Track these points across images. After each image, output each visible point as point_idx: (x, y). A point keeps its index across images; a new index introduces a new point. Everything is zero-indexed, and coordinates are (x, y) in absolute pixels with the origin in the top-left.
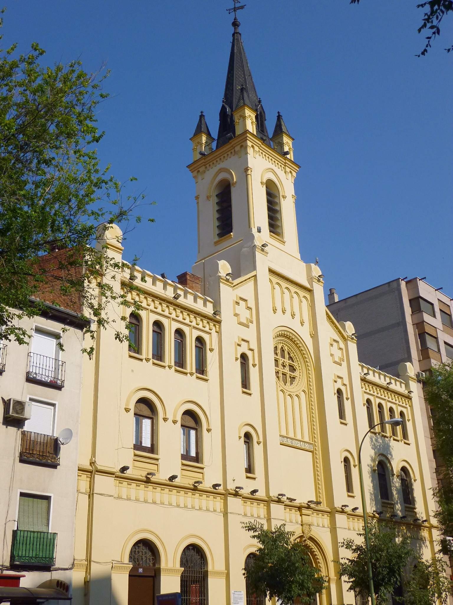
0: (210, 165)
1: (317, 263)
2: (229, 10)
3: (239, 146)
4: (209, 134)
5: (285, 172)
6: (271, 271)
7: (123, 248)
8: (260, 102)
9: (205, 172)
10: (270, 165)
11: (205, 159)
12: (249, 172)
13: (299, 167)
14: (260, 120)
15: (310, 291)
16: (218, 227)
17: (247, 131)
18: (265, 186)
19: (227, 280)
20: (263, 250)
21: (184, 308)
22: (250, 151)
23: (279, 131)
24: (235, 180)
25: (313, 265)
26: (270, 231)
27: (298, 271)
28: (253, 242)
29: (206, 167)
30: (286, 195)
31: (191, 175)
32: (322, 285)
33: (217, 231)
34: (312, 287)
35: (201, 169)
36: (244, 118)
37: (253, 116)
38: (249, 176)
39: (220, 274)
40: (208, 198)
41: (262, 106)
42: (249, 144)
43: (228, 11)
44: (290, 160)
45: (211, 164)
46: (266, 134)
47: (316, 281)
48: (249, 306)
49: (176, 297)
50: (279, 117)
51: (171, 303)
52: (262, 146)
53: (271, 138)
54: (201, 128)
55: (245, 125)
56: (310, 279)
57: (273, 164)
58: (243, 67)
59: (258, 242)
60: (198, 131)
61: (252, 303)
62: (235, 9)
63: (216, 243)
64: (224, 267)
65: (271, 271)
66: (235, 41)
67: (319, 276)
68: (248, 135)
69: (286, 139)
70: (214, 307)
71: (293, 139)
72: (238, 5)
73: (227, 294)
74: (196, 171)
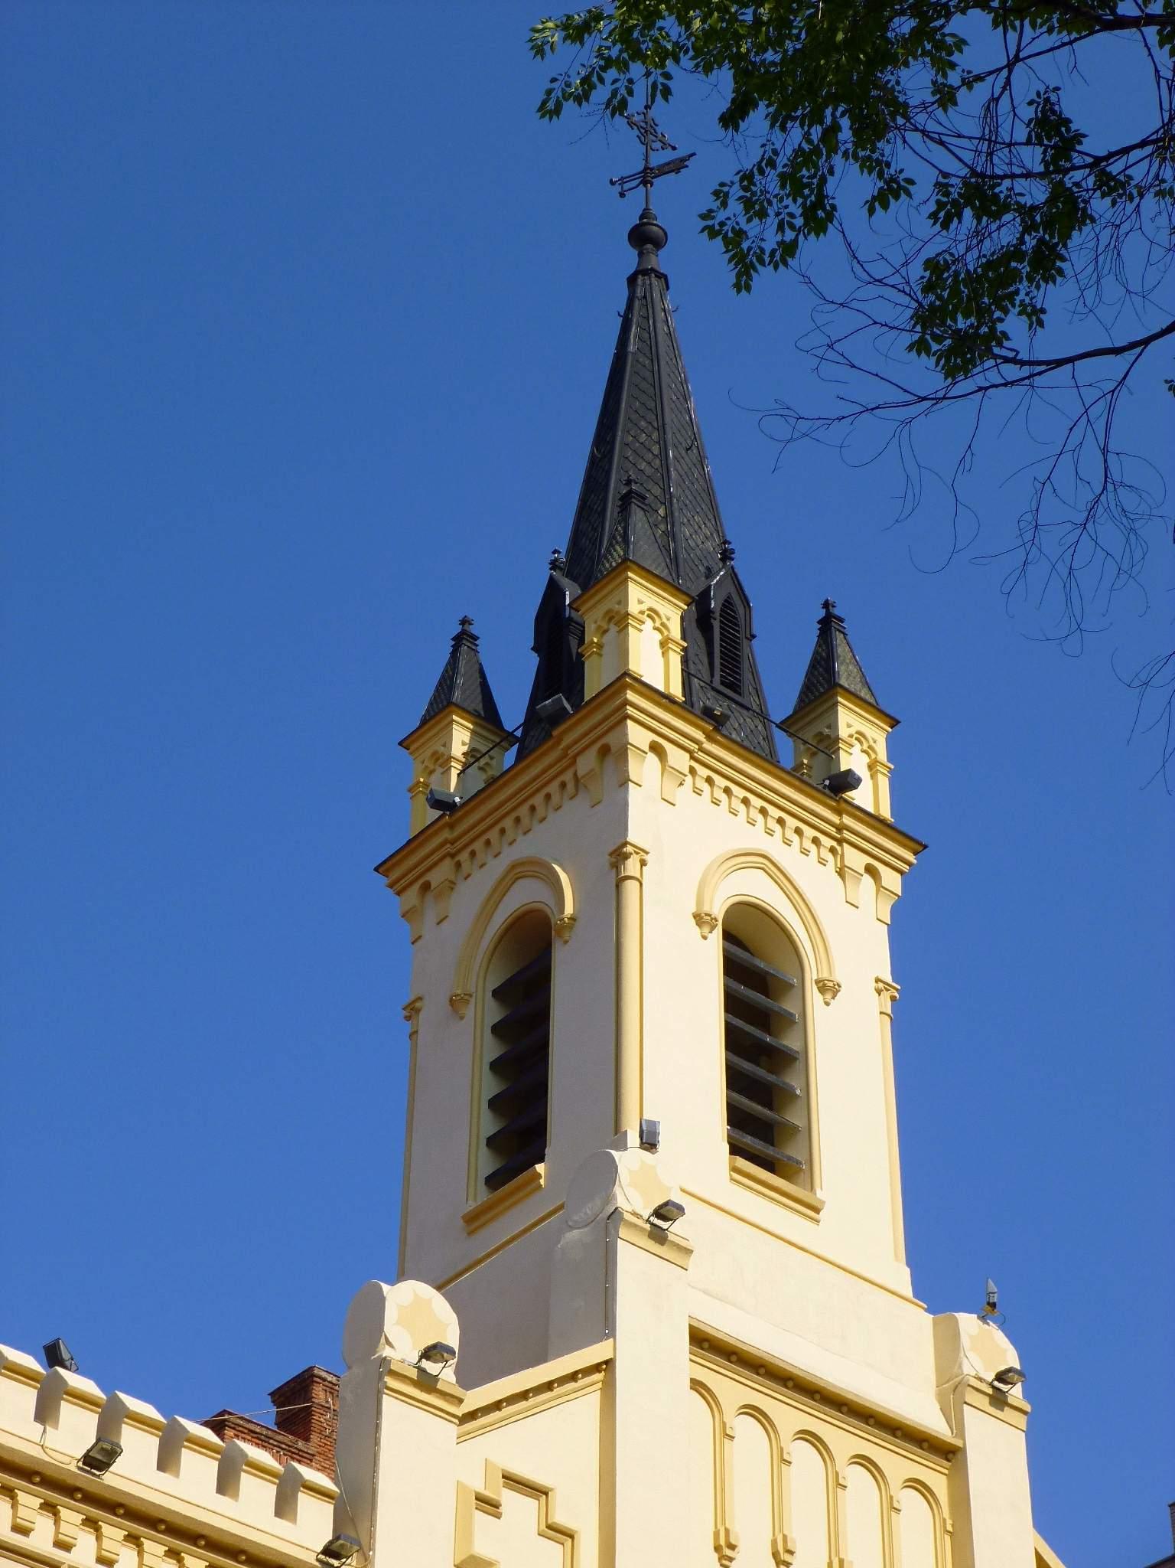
0: (473, 854)
1: (989, 1310)
2: (623, 180)
3: (592, 753)
4: (487, 716)
5: (841, 873)
6: (702, 1341)
7: (1028, 1408)
8: (727, 555)
9: (452, 885)
10: (756, 837)
11: (451, 826)
12: (632, 867)
13: (919, 847)
14: (718, 637)
15: (948, 1453)
16: (490, 1142)
17: (625, 679)
18: (716, 938)
19: (427, 1382)
20: (659, 1236)
21: (144, 1520)
22: (643, 769)
23: (820, 686)
24: (569, 909)
25: (968, 1322)
26: (735, 1150)
27: (889, 1347)
28: (609, 1197)
29: (458, 865)
30: (838, 977)
31: (397, 904)
32: (1022, 1421)
33: (487, 1163)
34: (959, 1429)
35: (436, 877)
36: (620, 620)
37: (673, 612)
38: (631, 886)
39: (387, 1352)
40: (456, 1003)
41: (733, 575)
42: (637, 735)
43: (618, 188)
44: (874, 820)
45: (478, 846)
46: (753, 702)
47: (984, 1402)
48: (560, 1518)
49: (100, 1458)
50: (829, 624)
51: (69, 1490)
52: (708, 746)
53: (761, 705)
54: (458, 687)
55: (623, 653)
56: (953, 1392)
57: (770, 833)
58: (659, 411)
59: (631, 1192)
60: (441, 706)
61: (577, 1508)
62: (646, 176)
63: (475, 1220)
64: (416, 1315)
65: (702, 1341)
66: (637, 303)
67: (1001, 1377)
68: (631, 696)
69: (849, 720)
70: (341, 1520)
71: (894, 722)
72: (658, 159)
73: (417, 1452)
74: (416, 886)
